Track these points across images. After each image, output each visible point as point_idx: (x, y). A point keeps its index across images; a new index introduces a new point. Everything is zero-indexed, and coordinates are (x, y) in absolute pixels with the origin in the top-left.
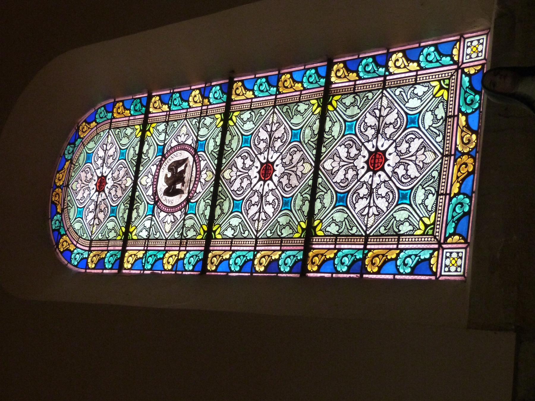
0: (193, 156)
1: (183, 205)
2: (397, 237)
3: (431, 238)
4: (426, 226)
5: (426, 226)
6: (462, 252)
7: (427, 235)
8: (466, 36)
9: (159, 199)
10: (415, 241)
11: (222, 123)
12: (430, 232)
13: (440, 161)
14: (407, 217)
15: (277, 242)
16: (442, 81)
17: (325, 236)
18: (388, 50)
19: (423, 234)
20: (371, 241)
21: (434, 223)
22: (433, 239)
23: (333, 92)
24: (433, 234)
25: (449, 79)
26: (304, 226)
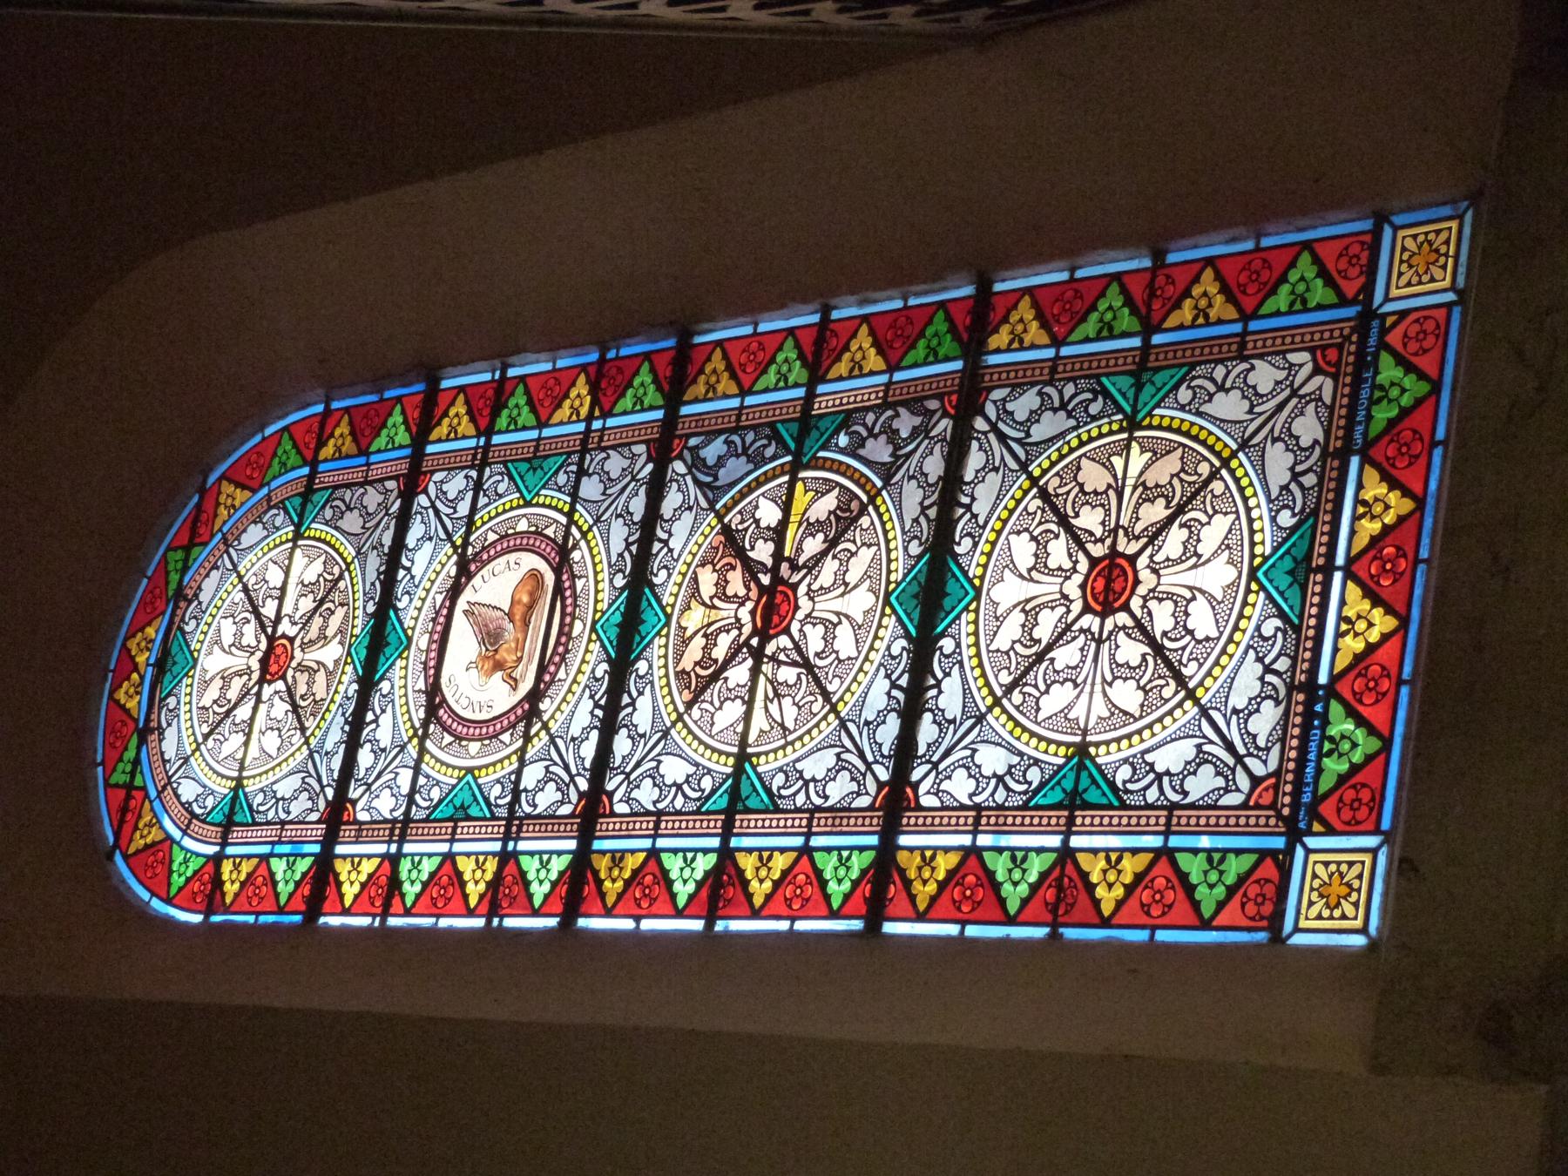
0: (558, 571)
1: (519, 712)
2: (1066, 813)
3: (1268, 817)
4: (1255, 781)
5: (1255, 781)
6: (1363, 863)
7: (1257, 806)
8: (1398, 220)
9: (444, 700)
10: (1247, 825)
11: (650, 467)
12: (1267, 799)
13: (1311, 521)
14: (1119, 682)
15: (797, 823)
16: (1319, 353)
17: (944, 808)
18: (1158, 255)
19: (1244, 806)
20: (1083, 825)
21: (1277, 774)
22: (1272, 821)
23: (987, 378)
24: (1273, 806)
25: (1340, 347)
26: (884, 775)
